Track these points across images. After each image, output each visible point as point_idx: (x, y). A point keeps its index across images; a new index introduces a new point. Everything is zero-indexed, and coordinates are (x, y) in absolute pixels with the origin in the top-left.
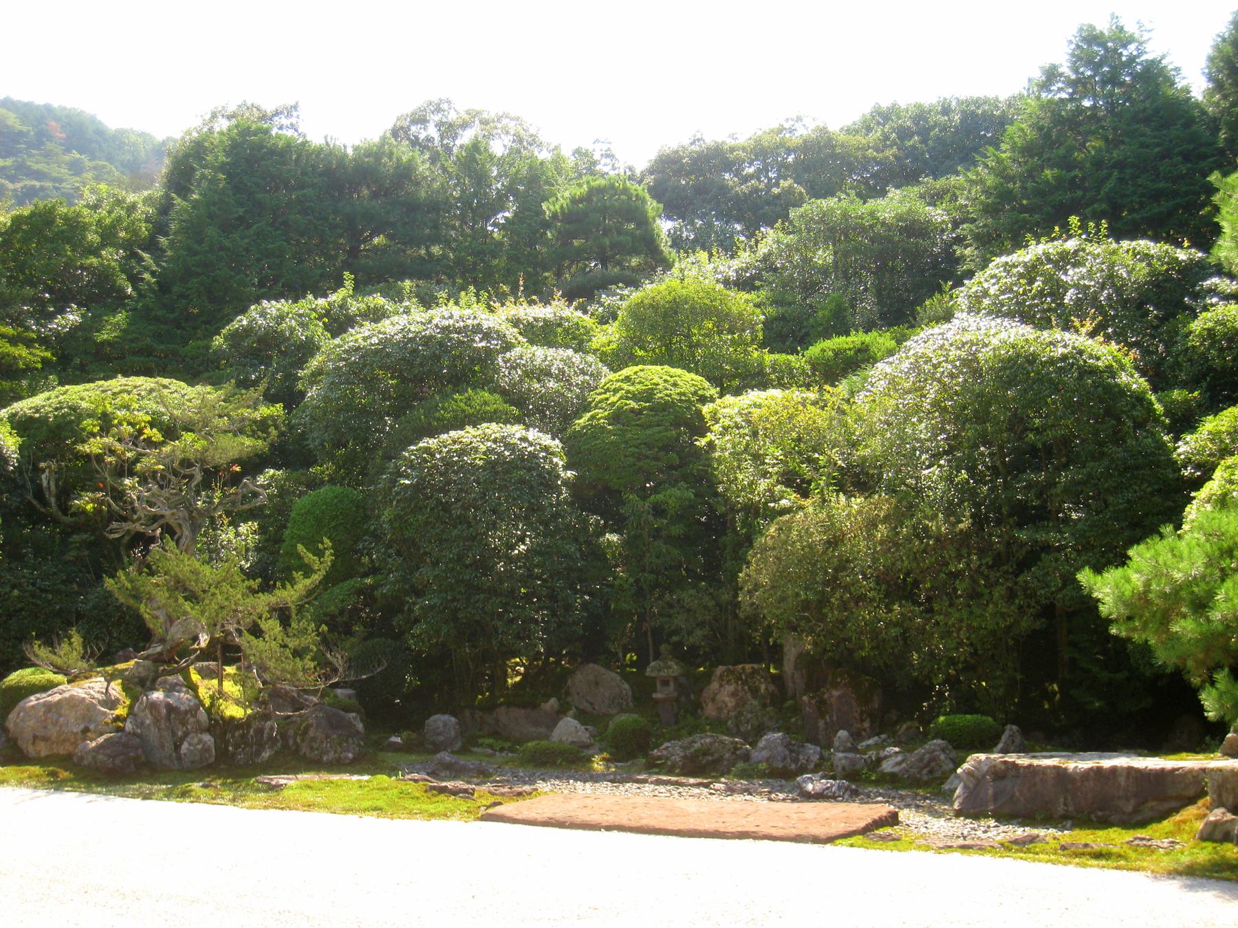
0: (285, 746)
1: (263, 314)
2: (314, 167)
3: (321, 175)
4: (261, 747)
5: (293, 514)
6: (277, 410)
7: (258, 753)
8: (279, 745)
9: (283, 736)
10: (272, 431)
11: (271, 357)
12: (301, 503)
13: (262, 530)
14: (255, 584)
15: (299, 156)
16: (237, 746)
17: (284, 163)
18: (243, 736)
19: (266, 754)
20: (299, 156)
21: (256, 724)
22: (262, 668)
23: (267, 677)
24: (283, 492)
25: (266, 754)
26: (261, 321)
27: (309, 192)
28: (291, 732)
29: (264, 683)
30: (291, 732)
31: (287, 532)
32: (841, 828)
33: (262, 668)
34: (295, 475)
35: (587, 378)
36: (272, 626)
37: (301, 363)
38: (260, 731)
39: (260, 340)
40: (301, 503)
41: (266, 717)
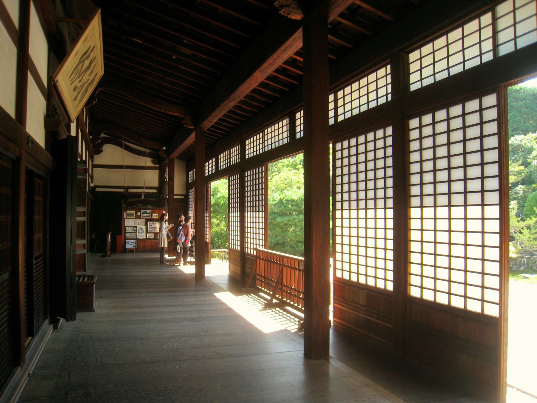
0: (528, 266)
1: (516, 140)
2: (529, 94)
3: (532, 95)
4: (521, 266)
5: (528, 199)
6: (522, 168)
7: (520, 268)
8: (526, 266)
9: (527, 263)
10: (523, 174)
11: (518, 153)
12: (531, 195)
13: (518, 203)
14: (519, 219)
15: (524, 91)
16: (513, 265)
17: (519, 93)
18: (515, 262)
19: (522, 268)
20: (524, 91)
21: (519, 259)
22: (521, 243)
23: (523, 246)
24: (524, 192)
25: (522, 268)
26: (515, 142)
27: (528, 101)
28: (530, 262)
29: (522, 247)
30: (530, 262)
31: (526, 204)
32: (96, 78)
33: (521, 243)
34: (528, 187)
35: (184, 222)
36: (526, 231)
37: (529, 154)
38: (521, 261)
39: (515, 147)
40: (531, 195)
41: (522, 257)
